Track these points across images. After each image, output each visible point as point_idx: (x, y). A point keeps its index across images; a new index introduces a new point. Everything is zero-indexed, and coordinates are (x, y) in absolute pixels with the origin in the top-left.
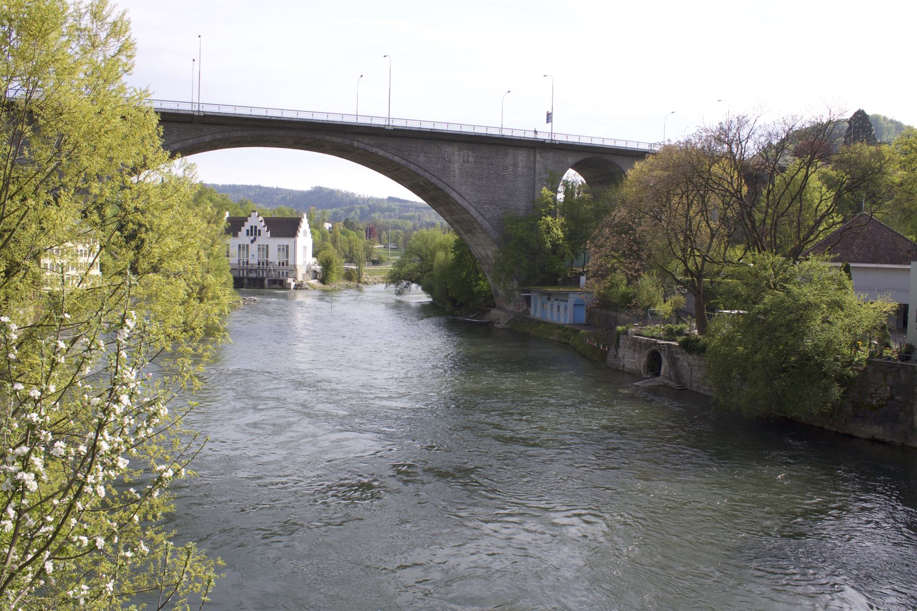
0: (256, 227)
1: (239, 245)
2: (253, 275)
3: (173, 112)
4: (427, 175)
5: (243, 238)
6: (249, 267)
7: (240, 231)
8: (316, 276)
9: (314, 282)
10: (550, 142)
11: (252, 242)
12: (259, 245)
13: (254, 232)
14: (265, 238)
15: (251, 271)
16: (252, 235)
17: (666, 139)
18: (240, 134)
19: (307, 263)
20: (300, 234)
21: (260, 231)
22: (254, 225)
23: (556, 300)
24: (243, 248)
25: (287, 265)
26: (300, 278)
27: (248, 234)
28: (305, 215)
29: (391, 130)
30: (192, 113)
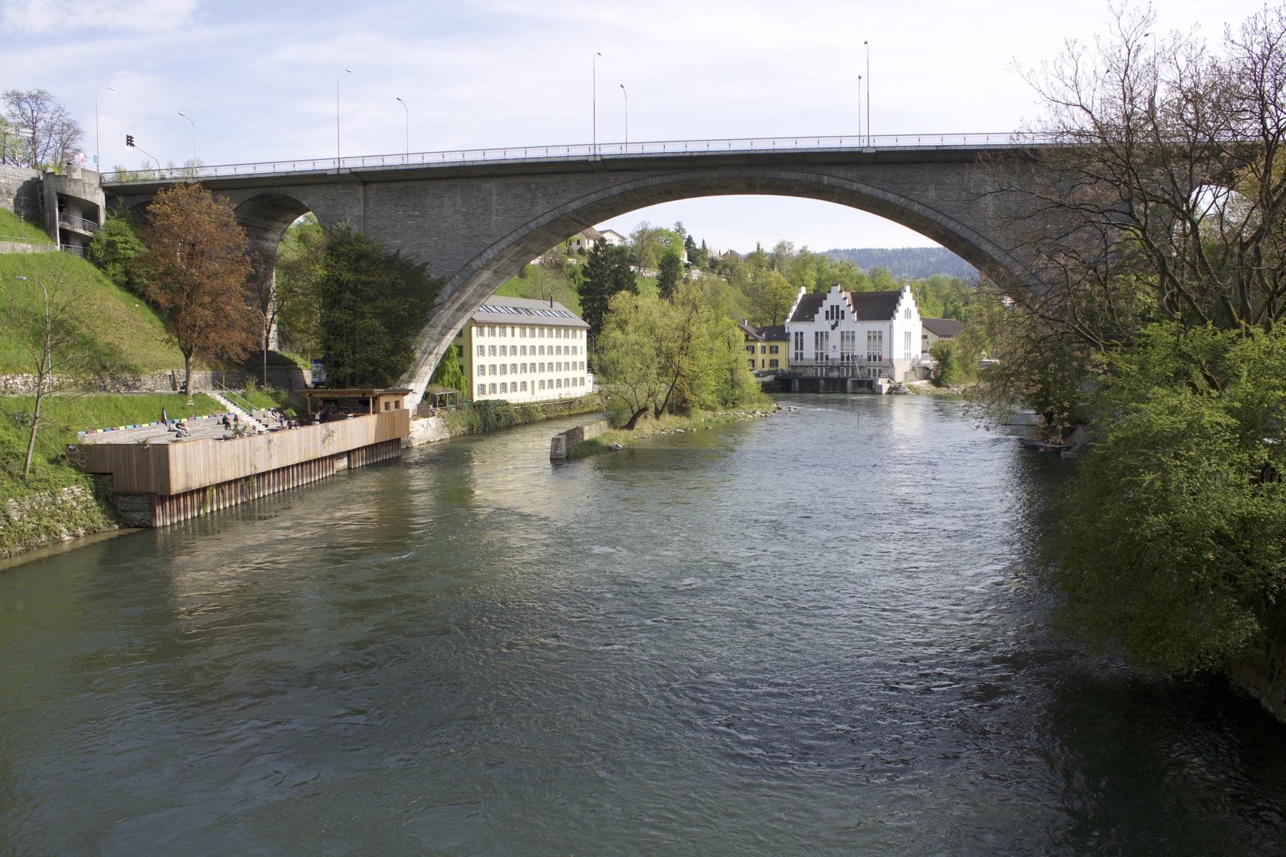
0: (838, 307)
1: (817, 333)
2: (835, 374)
3: (562, 159)
4: (940, 217)
5: (821, 322)
6: (830, 363)
7: (817, 313)
8: (929, 374)
9: (922, 384)
10: (335, 172)
11: (833, 328)
12: (842, 333)
13: (836, 314)
15: (831, 368)
16: (832, 318)
18: (658, 180)
19: (913, 357)
21: (843, 312)
22: (835, 304)
24: (848, 337)
25: (880, 358)
26: (899, 377)
27: (827, 318)
28: (908, 288)
29: (872, 154)
30: (860, 150)
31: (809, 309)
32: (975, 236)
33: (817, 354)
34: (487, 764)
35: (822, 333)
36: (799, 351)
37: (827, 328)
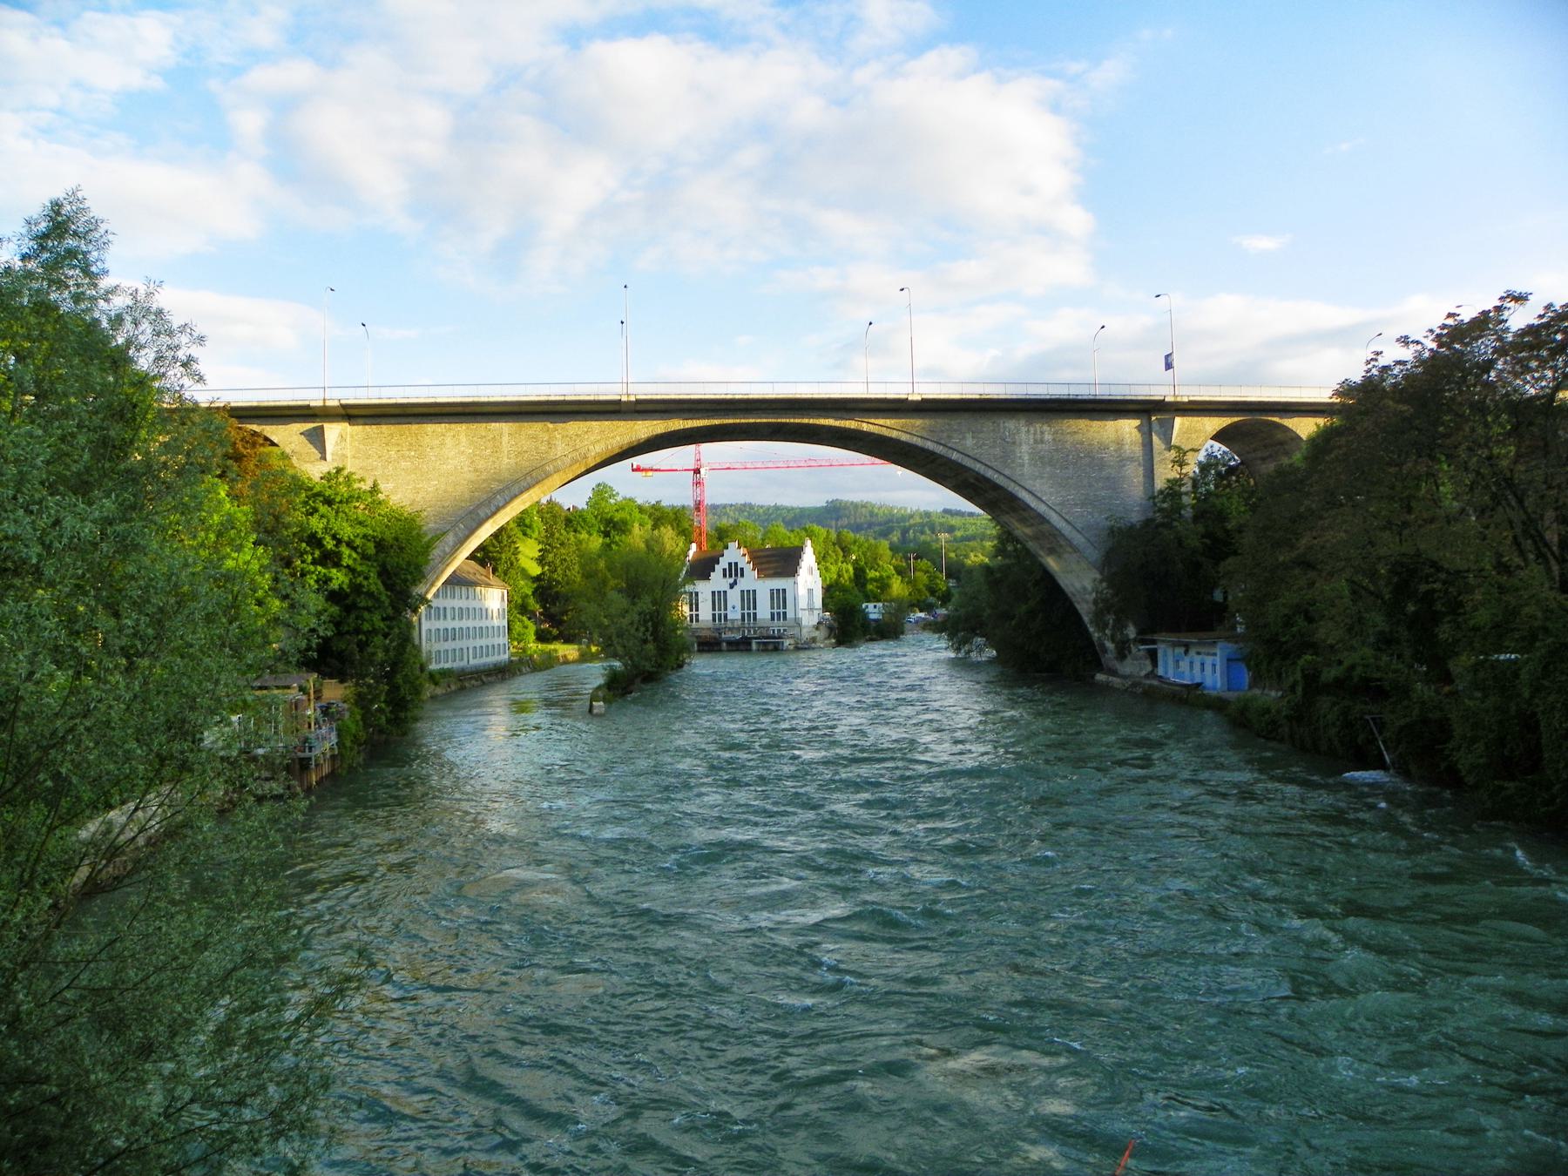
0: (736, 564)
1: (713, 593)
5: (717, 581)
11: (732, 586)
12: (742, 592)
13: (734, 571)
16: (731, 576)
21: (742, 569)
23: (1198, 653)
27: (725, 576)
31: (703, 569)
32: (1012, 484)
33: (714, 615)
34: (1250, 954)
35: (778, 590)
36: (694, 613)
37: (727, 588)
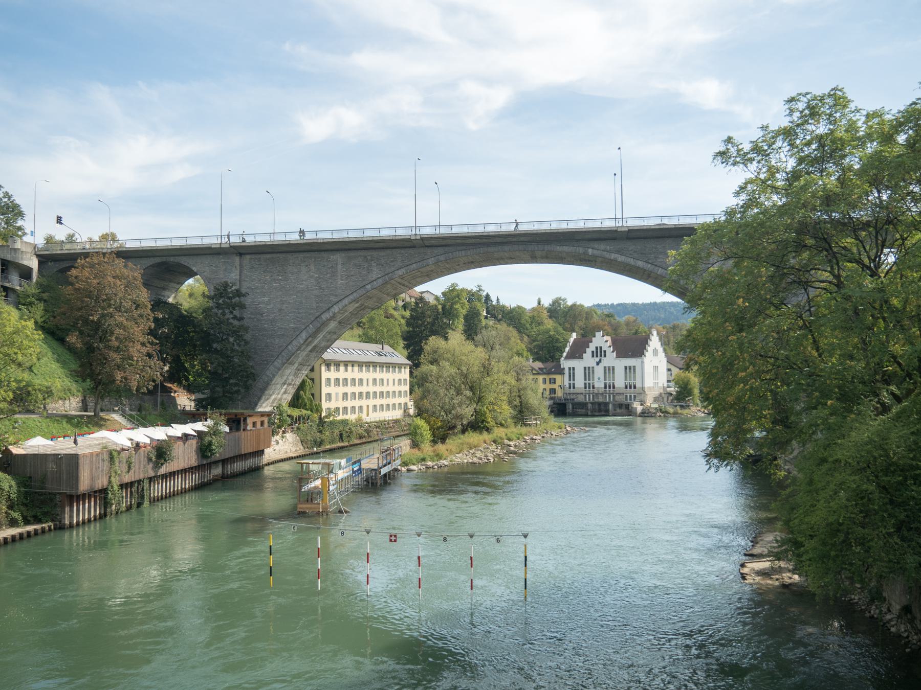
0: (601, 348)
3: (391, 238)
6: (596, 391)
11: (598, 364)
12: (605, 367)
13: (599, 353)
14: (611, 359)
17: (225, 233)
20: (649, 353)
21: (605, 352)
24: (609, 369)
25: (635, 387)
27: (593, 356)
28: (655, 333)
